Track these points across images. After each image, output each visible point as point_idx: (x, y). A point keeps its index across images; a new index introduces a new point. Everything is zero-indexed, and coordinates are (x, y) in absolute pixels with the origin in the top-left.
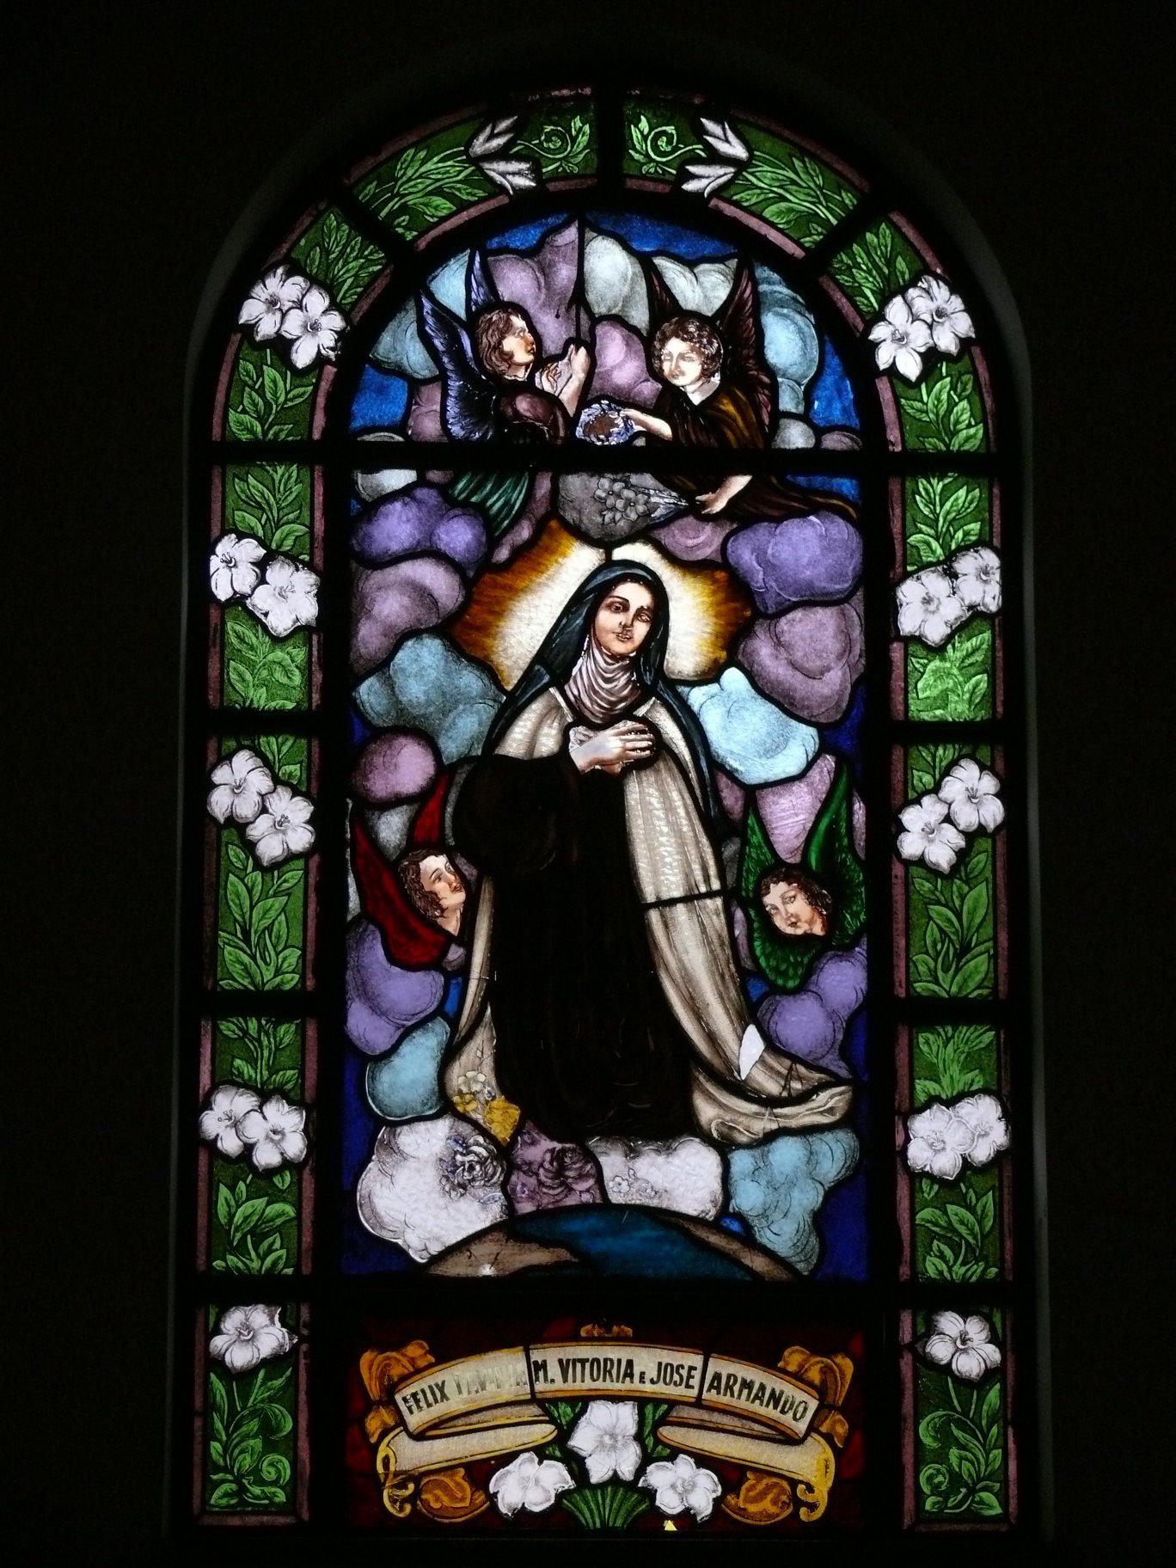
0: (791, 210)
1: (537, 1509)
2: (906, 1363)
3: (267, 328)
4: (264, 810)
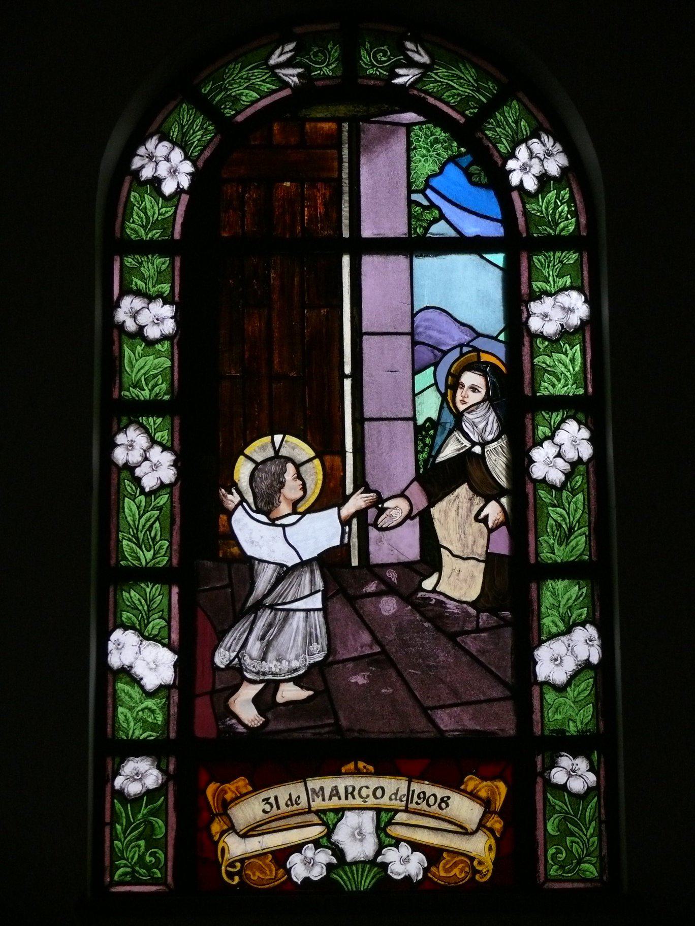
0: (459, 95)
1: (316, 879)
2: (539, 780)
3: (147, 173)
4: (146, 459)
